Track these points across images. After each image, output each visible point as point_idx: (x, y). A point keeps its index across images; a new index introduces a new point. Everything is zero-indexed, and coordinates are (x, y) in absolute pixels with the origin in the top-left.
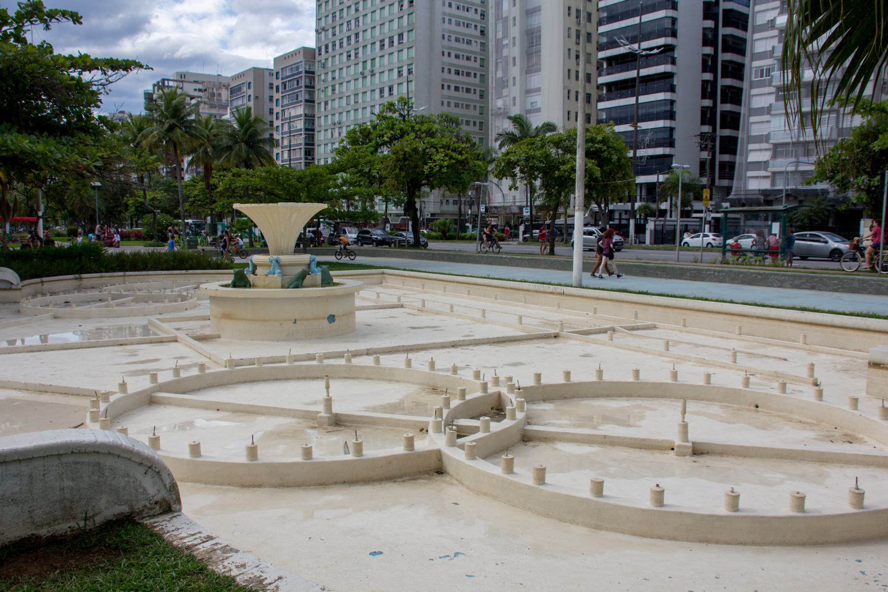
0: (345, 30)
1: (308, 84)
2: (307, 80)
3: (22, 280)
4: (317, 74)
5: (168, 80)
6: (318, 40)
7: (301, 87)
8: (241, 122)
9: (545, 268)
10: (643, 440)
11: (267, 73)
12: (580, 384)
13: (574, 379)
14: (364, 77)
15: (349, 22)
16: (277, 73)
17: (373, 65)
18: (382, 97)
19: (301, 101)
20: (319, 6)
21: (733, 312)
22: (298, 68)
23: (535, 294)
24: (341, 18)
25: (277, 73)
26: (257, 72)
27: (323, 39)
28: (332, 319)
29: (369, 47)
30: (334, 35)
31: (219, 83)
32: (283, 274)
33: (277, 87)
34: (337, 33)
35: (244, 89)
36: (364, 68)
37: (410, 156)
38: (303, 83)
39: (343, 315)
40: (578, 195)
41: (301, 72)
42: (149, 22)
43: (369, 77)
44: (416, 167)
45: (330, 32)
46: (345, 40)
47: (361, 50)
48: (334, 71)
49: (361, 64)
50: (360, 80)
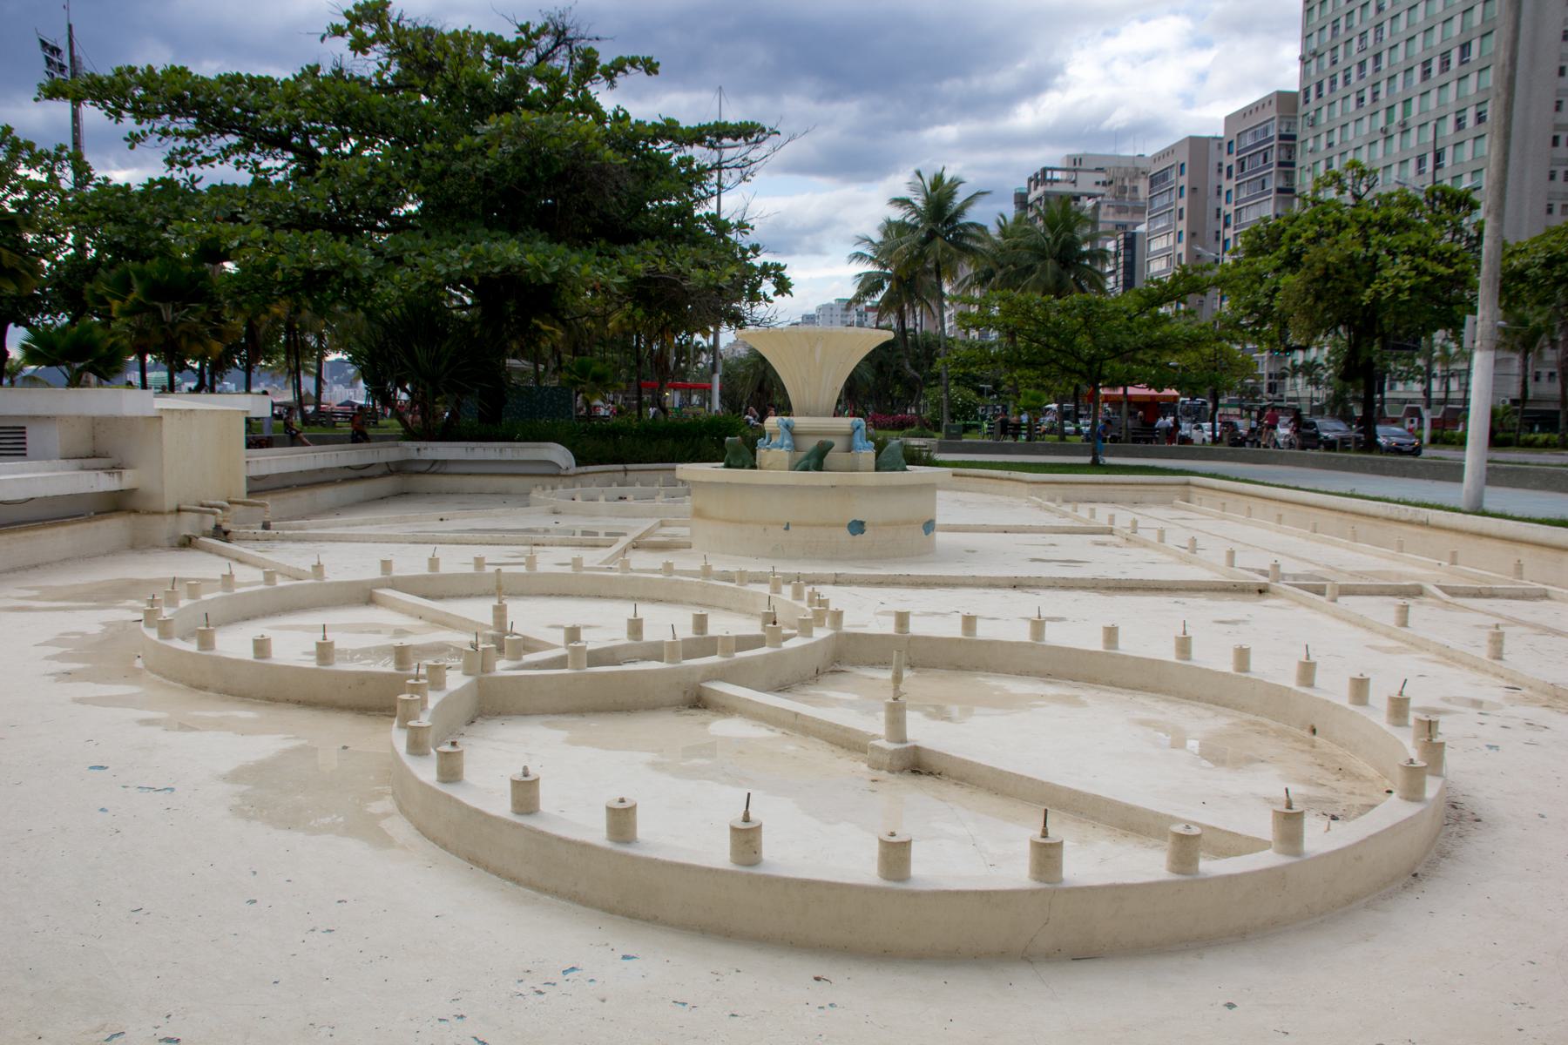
0: (1354, 51)
1: (1284, 159)
2: (1283, 153)
3: (578, 464)
4: (1299, 139)
5: (1052, 169)
6: (1305, 74)
7: (1270, 166)
8: (1051, 225)
9: (1535, 488)
10: (846, 730)
11: (1213, 146)
12: (990, 643)
13: (984, 631)
14: (1388, 138)
15: (1363, 35)
16: (1230, 143)
17: (1406, 113)
18: (1421, 173)
19: (1270, 192)
20: (1308, 11)
21: (1525, 538)
22: (1266, 131)
23: (1386, 524)
24: (1348, 28)
25: (1230, 143)
26: (1197, 144)
27: (1313, 72)
28: (857, 527)
29: (1400, 78)
30: (1334, 63)
31: (1135, 170)
32: (795, 448)
33: (1229, 169)
34: (1340, 58)
35: (1173, 176)
36: (1389, 119)
37: (1338, 272)
38: (1273, 158)
39: (885, 524)
40: (1484, 318)
41: (1271, 139)
42: (1063, 74)
43: (1397, 137)
44: (1349, 292)
45: (1327, 58)
46: (1354, 71)
47: (1383, 87)
48: (1330, 132)
49: (1382, 114)
50: (1381, 143)
